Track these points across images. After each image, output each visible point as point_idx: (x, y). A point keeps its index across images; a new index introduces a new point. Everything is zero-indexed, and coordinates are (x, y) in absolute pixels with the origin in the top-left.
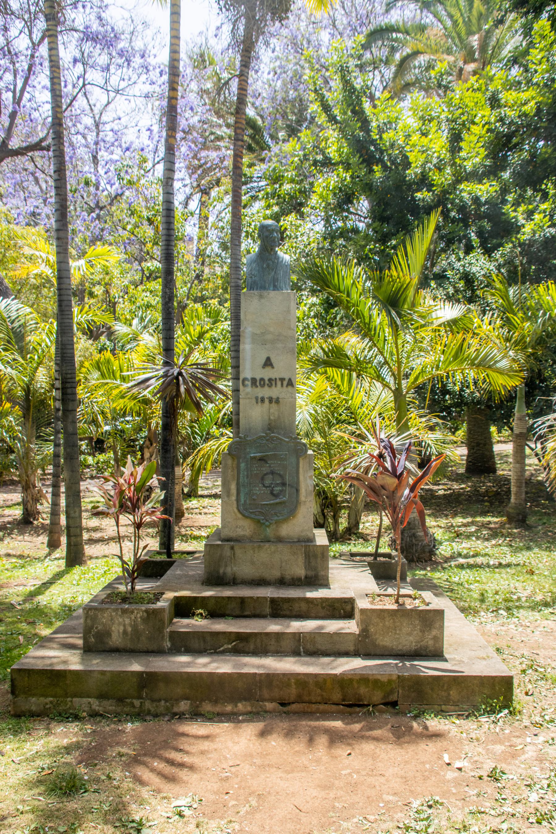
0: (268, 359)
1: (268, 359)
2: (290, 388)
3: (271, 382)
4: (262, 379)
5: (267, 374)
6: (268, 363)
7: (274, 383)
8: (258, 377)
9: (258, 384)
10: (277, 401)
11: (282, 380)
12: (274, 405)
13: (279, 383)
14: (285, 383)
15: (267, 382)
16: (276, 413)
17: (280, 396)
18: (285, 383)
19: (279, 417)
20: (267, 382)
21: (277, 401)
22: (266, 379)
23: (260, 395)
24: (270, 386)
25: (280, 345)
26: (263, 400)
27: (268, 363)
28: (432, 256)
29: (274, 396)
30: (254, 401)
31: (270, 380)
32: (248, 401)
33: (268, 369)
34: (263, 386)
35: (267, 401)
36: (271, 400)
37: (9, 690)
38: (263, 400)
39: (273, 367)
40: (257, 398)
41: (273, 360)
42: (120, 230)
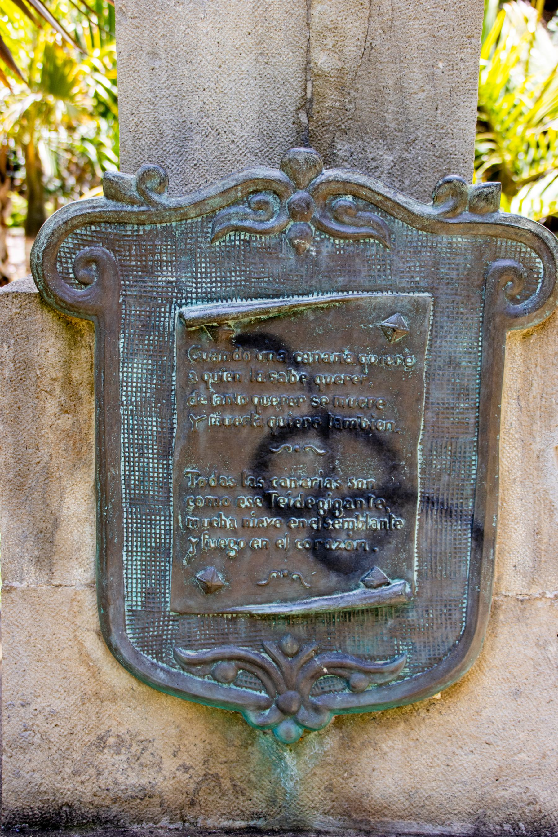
16: (354, 28)
19: (368, 51)
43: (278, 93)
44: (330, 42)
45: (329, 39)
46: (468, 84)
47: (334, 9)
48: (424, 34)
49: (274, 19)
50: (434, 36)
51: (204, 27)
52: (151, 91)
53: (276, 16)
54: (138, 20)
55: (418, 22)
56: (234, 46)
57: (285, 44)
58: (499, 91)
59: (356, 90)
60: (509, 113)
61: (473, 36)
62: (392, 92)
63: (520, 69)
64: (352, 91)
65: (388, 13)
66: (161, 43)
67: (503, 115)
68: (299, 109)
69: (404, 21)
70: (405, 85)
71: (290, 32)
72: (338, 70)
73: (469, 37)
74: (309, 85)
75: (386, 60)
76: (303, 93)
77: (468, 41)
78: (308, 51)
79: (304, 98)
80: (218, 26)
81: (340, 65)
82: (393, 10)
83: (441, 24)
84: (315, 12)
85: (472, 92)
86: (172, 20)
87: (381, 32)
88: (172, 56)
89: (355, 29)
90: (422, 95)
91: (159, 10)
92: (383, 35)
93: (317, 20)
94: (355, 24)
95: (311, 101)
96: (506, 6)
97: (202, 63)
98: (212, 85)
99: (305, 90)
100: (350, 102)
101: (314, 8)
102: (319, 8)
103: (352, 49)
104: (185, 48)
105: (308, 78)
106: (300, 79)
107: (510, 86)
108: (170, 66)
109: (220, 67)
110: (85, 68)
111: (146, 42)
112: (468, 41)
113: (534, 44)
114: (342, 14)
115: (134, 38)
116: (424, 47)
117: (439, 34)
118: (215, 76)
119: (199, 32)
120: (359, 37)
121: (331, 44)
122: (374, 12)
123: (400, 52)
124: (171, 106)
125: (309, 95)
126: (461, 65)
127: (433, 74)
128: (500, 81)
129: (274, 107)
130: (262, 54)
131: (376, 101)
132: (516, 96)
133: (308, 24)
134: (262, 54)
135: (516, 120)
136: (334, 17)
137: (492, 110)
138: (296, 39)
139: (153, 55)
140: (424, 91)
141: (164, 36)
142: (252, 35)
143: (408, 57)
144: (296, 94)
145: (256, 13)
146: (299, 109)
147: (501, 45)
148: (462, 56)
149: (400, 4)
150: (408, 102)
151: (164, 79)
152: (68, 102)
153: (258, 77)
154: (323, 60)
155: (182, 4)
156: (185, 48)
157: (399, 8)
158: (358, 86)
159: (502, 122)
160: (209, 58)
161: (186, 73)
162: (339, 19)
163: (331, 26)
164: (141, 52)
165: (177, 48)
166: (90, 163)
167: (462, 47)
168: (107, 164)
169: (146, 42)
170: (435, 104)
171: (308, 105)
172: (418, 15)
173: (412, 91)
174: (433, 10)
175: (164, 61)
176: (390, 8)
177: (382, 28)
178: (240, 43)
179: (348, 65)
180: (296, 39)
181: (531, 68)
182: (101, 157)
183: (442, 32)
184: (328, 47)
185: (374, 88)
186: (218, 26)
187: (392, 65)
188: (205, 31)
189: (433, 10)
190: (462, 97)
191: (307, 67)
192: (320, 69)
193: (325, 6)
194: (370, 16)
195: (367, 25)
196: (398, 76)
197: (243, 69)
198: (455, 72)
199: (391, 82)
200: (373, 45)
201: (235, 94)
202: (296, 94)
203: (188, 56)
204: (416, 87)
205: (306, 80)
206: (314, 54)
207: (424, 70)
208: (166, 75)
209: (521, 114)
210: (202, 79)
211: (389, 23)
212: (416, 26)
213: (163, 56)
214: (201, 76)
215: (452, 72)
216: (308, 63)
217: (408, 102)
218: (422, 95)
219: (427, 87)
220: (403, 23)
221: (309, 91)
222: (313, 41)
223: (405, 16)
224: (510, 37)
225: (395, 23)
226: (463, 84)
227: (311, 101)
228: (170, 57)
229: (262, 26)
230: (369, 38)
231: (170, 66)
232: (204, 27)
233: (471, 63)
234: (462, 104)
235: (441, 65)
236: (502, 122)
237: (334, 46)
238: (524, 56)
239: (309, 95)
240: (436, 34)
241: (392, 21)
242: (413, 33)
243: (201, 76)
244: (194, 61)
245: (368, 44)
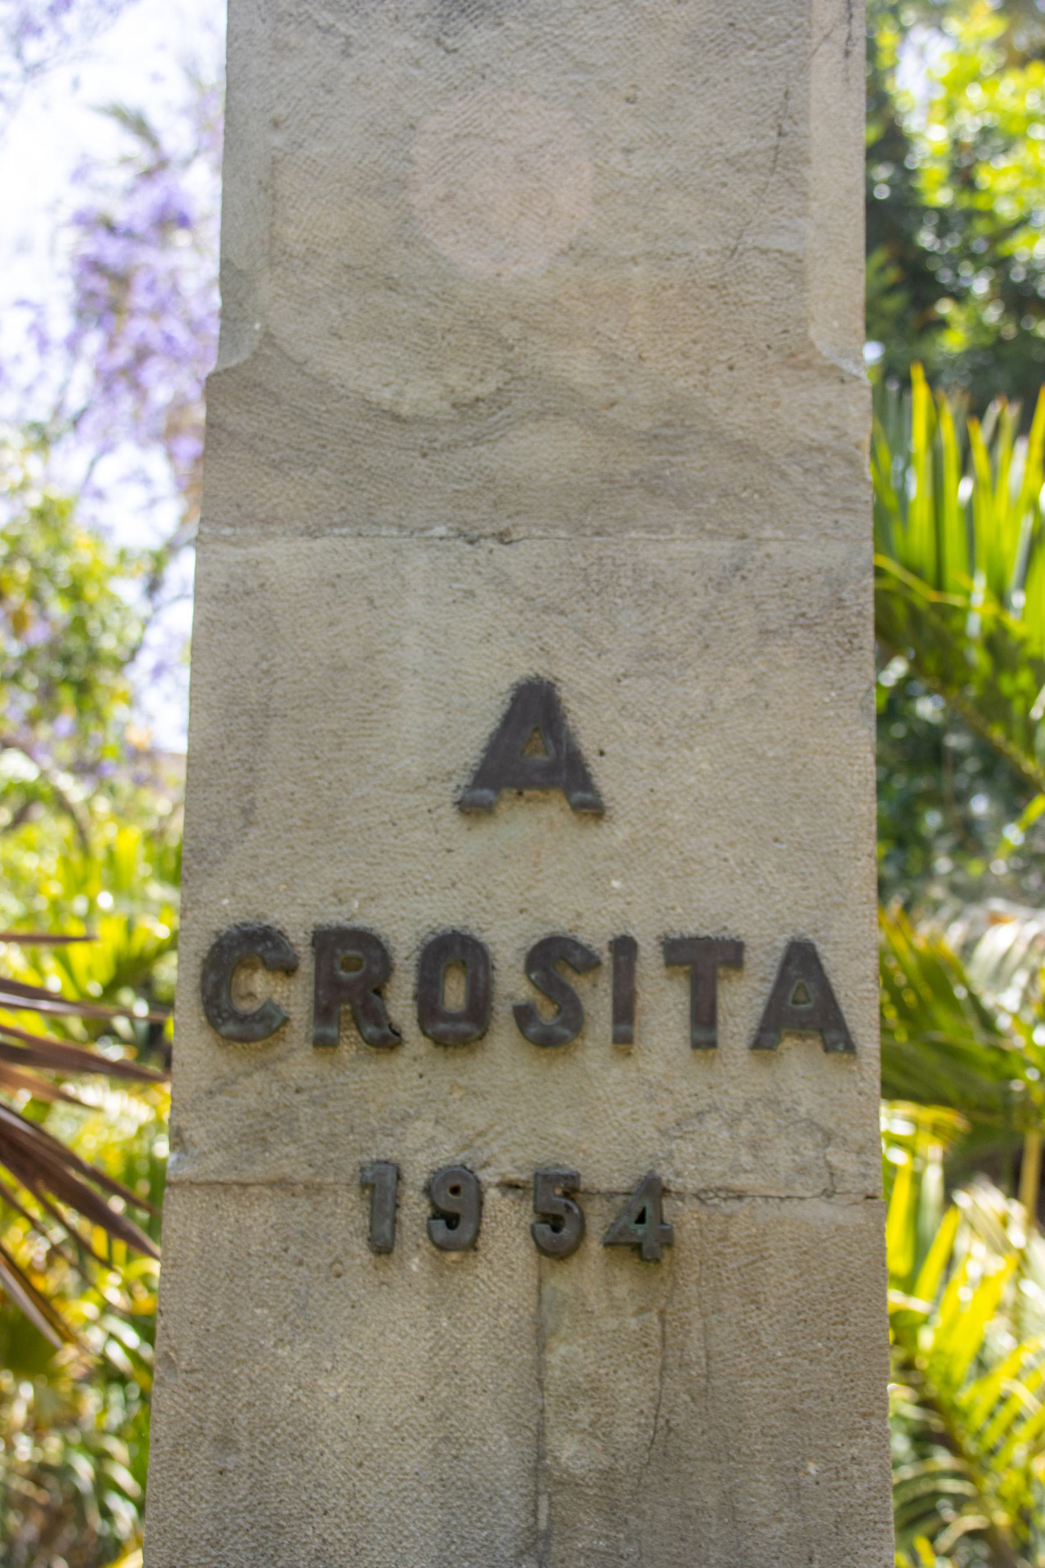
0: (535, 709)
1: (535, 709)
2: (799, 1060)
3: (568, 988)
4: (453, 951)
5: (524, 877)
6: (534, 753)
7: (597, 1000)
8: (406, 926)
9: (401, 1004)
10: (644, 1231)
11: (701, 961)
12: (592, 1277)
13: (663, 1001)
14: (742, 1001)
15: (512, 984)
16: (631, 1390)
17: (684, 1171)
18: (742, 1001)
19: (663, 1441)
20: (512, 984)
21: (644, 1231)
22: (507, 945)
23: (423, 1154)
24: (552, 1031)
25: (678, 550)
26: (455, 1211)
27: (534, 753)
28: (804, 1003)
29: (607, 1165)
30: (346, 1215)
31: (554, 958)
32: (262, 1216)
33: (533, 824)
34: (459, 1032)
35: (507, 1225)
36: (558, 1211)
37: (553, 1342)
38: (455, 1211)
39: (591, 808)
40: (379, 1187)
41: (589, 724)
42: (664, 294)
43: (479, 1520)
44: (584, 1415)
45: (582, 1411)
46: (872, 1510)
47: (592, 1353)
48: (775, 1405)
49: (472, 1371)
50: (794, 1411)
51: (331, 1387)
52: (215, 1517)
53: (476, 1366)
54: (200, 1376)
55: (759, 1381)
56: (390, 1424)
57: (493, 1419)
58: (962, 1367)
59: (641, 1515)
60: (991, 1415)
61: (872, 1414)
62: (714, 1521)
63: (1002, 1323)
64: (631, 1517)
65: (698, 1363)
66: (243, 1419)
67: (978, 1418)
68: (522, 1553)
69: (732, 1378)
70: (741, 1506)
71: (503, 1396)
72: (601, 1472)
73: (864, 1415)
74: (543, 1502)
75: (699, 1455)
76: (531, 1520)
77: (864, 1423)
78: (540, 1434)
79: (532, 1530)
80: (360, 1384)
81: (605, 1461)
82: (708, 1357)
83: (807, 1387)
84: (553, 1359)
85: (881, 1526)
86: (267, 1374)
87: (687, 1398)
88: (263, 1444)
89: (634, 1392)
90: (779, 1529)
91: (242, 1356)
92: (692, 1405)
93: (557, 1373)
94: (634, 1383)
95: (547, 1536)
96: (962, 1199)
97: (324, 1459)
98: (343, 1502)
99: (535, 1513)
100: (628, 1539)
101: (551, 1351)
102: (563, 1350)
103: (628, 1431)
104: (290, 1429)
105: (542, 1487)
106: (523, 1491)
107: (988, 1355)
108: (257, 1465)
109: (360, 1465)
110: (88, 1308)
111: (213, 1418)
112: (864, 1423)
113: (1025, 1271)
114: (607, 1362)
115: (188, 1410)
116: (775, 1431)
117: (804, 1406)
118: (349, 1485)
119: (320, 1396)
120: (644, 1407)
121: (587, 1420)
122: (671, 1360)
123: (727, 1438)
124: (254, 1549)
125: (543, 1525)
126: (854, 1470)
127: (798, 1486)
128: (963, 1349)
129: (470, 1548)
130: (446, 1439)
131: (683, 1539)
132: (1001, 1381)
133: (540, 1382)
134: (446, 1439)
135: (1008, 1432)
136: (591, 1368)
137: (954, 1408)
138: (517, 1410)
139: (225, 1443)
140: (781, 1520)
141: (250, 1405)
142: (428, 1401)
143: (744, 1449)
144: (515, 1522)
145: (436, 1360)
146: (522, 1553)
147: (957, 1276)
148: (854, 1451)
149: (722, 1348)
150: (749, 1543)
151: (243, 1492)
152: (43, 1381)
153: (438, 1486)
154: (569, 1451)
155: (290, 1343)
156: (290, 1429)
157: (721, 1354)
158: (645, 1506)
159: (979, 1435)
160: (339, 1447)
161: (290, 1478)
162: (602, 1371)
163: (586, 1386)
164: (200, 1439)
165: (274, 1428)
166: (77, 1497)
167: (852, 1433)
168: (115, 1502)
169: (213, 1418)
170: (805, 1549)
171: (540, 1546)
172: (759, 1369)
173: (757, 1520)
174: (787, 1360)
175: (245, 1456)
176: (701, 1353)
177: (688, 1392)
178: (402, 1417)
179: (622, 1463)
180: (517, 1410)
181: (1029, 1321)
182: (103, 1483)
183: (809, 1403)
184: (581, 1426)
185: (678, 1510)
186: (360, 1384)
187: (713, 1466)
188: (332, 1394)
189: (787, 1360)
190: (861, 1537)
191: (539, 1466)
192: (566, 1471)
193: (575, 1348)
194: (664, 1367)
195: (657, 1385)
196: (726, 1487)
197: (408, 1468)
198: (843, 1483)
199: (711, 1500)
200: (673, 1423)
201: (389, 1521)
202: (515, 1522)
203: (295, 1445)
204: (765, 1511)
205: (538, 1493)
206: (552, 1441)
207: (778, 1477)
208: (249, 1483)
209: (1019, 1418)
210: (323, 1491)
211: (703, 1381)
212: (757, 1390)
213: (245, 1444)
214: (320, 1485)
215: (835, 1484)
216: (541, 1457)
217: (749, 1543)
218: (779, 1529)
219: (787, 1513)
220: (730, 1383)
221: (543, 1516)
222: (550, 1414)
223: (733, 1370)
224: (978, 1259)
225: (717, 1383)
226: (862, 1510)
227: (547, 1536)
228: (258, 1447)
229: (448, 1385)
230: (663, 1411)
231: (257, 1465)
232: (331, 1387)
233: (874, 1468)
234: (863, 1552)
235: (812, 1468)
236: (979, 1435)
237: (592, 1424)
238: (1007, 1293)
239: (543, 1525)
240: (798, 1407)
241: (708, 1377)
242: (752, 1403)
243: (320, 1485)
244: (307, 1455)
245: (662, 1422)
